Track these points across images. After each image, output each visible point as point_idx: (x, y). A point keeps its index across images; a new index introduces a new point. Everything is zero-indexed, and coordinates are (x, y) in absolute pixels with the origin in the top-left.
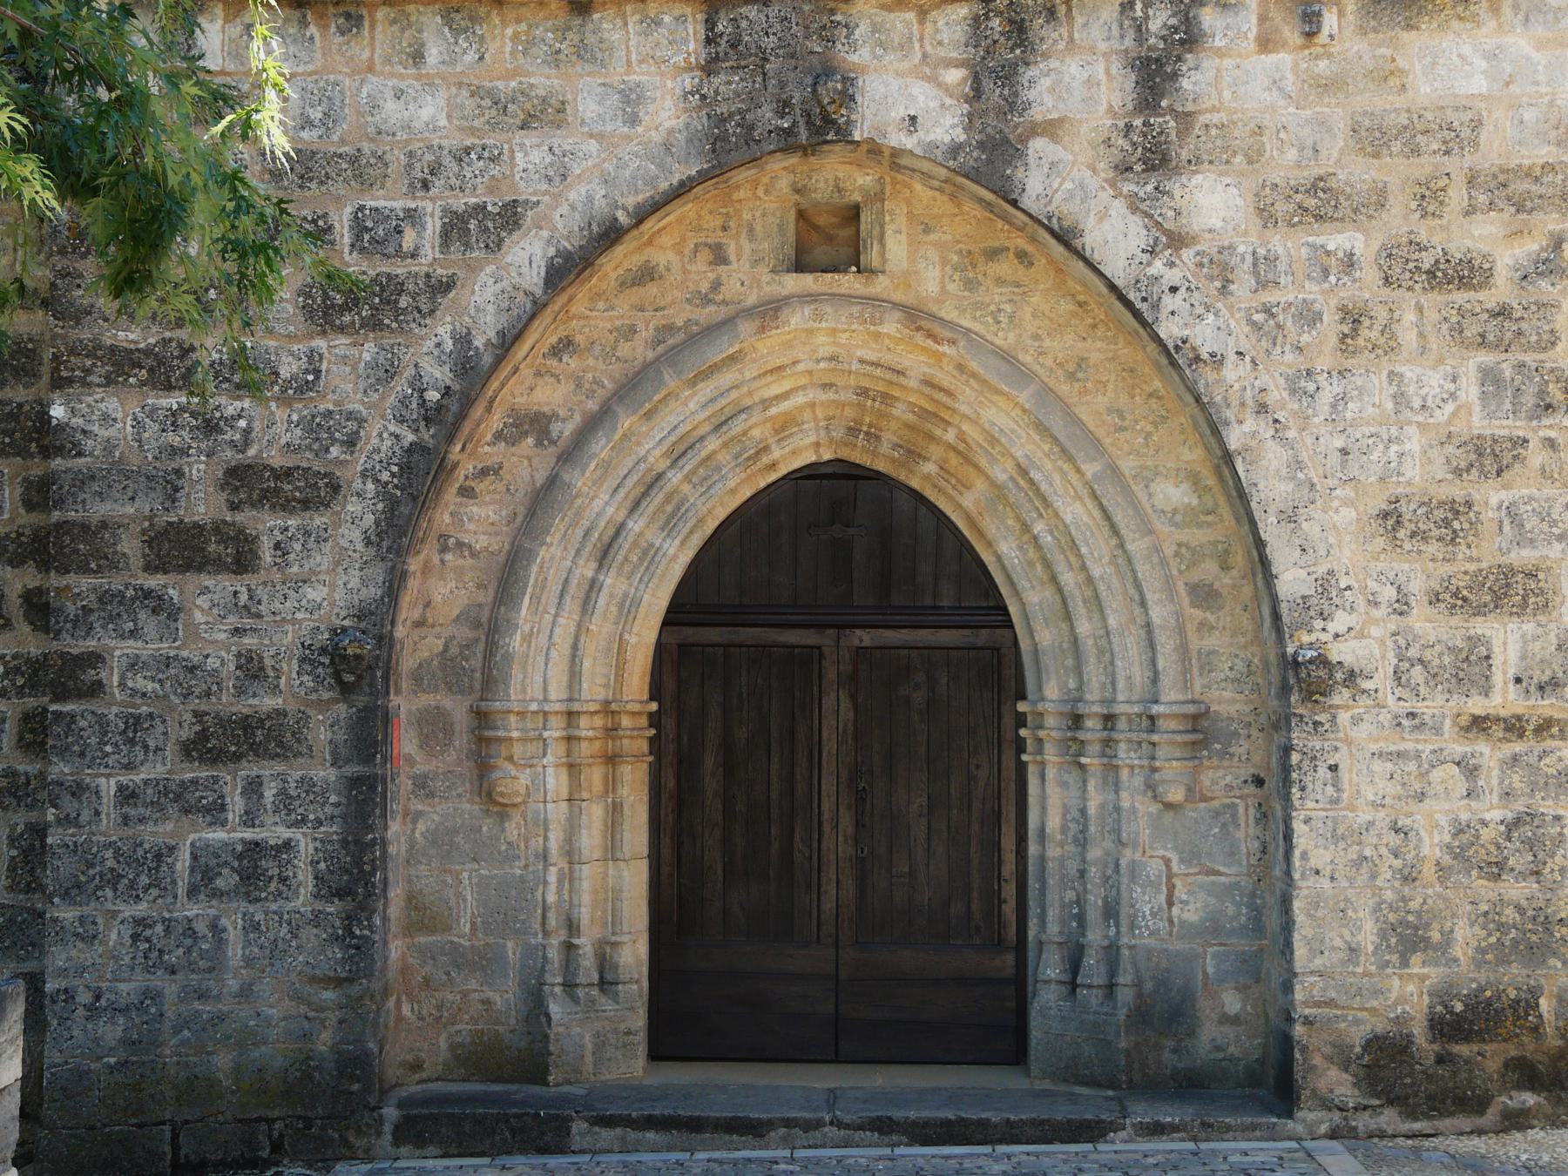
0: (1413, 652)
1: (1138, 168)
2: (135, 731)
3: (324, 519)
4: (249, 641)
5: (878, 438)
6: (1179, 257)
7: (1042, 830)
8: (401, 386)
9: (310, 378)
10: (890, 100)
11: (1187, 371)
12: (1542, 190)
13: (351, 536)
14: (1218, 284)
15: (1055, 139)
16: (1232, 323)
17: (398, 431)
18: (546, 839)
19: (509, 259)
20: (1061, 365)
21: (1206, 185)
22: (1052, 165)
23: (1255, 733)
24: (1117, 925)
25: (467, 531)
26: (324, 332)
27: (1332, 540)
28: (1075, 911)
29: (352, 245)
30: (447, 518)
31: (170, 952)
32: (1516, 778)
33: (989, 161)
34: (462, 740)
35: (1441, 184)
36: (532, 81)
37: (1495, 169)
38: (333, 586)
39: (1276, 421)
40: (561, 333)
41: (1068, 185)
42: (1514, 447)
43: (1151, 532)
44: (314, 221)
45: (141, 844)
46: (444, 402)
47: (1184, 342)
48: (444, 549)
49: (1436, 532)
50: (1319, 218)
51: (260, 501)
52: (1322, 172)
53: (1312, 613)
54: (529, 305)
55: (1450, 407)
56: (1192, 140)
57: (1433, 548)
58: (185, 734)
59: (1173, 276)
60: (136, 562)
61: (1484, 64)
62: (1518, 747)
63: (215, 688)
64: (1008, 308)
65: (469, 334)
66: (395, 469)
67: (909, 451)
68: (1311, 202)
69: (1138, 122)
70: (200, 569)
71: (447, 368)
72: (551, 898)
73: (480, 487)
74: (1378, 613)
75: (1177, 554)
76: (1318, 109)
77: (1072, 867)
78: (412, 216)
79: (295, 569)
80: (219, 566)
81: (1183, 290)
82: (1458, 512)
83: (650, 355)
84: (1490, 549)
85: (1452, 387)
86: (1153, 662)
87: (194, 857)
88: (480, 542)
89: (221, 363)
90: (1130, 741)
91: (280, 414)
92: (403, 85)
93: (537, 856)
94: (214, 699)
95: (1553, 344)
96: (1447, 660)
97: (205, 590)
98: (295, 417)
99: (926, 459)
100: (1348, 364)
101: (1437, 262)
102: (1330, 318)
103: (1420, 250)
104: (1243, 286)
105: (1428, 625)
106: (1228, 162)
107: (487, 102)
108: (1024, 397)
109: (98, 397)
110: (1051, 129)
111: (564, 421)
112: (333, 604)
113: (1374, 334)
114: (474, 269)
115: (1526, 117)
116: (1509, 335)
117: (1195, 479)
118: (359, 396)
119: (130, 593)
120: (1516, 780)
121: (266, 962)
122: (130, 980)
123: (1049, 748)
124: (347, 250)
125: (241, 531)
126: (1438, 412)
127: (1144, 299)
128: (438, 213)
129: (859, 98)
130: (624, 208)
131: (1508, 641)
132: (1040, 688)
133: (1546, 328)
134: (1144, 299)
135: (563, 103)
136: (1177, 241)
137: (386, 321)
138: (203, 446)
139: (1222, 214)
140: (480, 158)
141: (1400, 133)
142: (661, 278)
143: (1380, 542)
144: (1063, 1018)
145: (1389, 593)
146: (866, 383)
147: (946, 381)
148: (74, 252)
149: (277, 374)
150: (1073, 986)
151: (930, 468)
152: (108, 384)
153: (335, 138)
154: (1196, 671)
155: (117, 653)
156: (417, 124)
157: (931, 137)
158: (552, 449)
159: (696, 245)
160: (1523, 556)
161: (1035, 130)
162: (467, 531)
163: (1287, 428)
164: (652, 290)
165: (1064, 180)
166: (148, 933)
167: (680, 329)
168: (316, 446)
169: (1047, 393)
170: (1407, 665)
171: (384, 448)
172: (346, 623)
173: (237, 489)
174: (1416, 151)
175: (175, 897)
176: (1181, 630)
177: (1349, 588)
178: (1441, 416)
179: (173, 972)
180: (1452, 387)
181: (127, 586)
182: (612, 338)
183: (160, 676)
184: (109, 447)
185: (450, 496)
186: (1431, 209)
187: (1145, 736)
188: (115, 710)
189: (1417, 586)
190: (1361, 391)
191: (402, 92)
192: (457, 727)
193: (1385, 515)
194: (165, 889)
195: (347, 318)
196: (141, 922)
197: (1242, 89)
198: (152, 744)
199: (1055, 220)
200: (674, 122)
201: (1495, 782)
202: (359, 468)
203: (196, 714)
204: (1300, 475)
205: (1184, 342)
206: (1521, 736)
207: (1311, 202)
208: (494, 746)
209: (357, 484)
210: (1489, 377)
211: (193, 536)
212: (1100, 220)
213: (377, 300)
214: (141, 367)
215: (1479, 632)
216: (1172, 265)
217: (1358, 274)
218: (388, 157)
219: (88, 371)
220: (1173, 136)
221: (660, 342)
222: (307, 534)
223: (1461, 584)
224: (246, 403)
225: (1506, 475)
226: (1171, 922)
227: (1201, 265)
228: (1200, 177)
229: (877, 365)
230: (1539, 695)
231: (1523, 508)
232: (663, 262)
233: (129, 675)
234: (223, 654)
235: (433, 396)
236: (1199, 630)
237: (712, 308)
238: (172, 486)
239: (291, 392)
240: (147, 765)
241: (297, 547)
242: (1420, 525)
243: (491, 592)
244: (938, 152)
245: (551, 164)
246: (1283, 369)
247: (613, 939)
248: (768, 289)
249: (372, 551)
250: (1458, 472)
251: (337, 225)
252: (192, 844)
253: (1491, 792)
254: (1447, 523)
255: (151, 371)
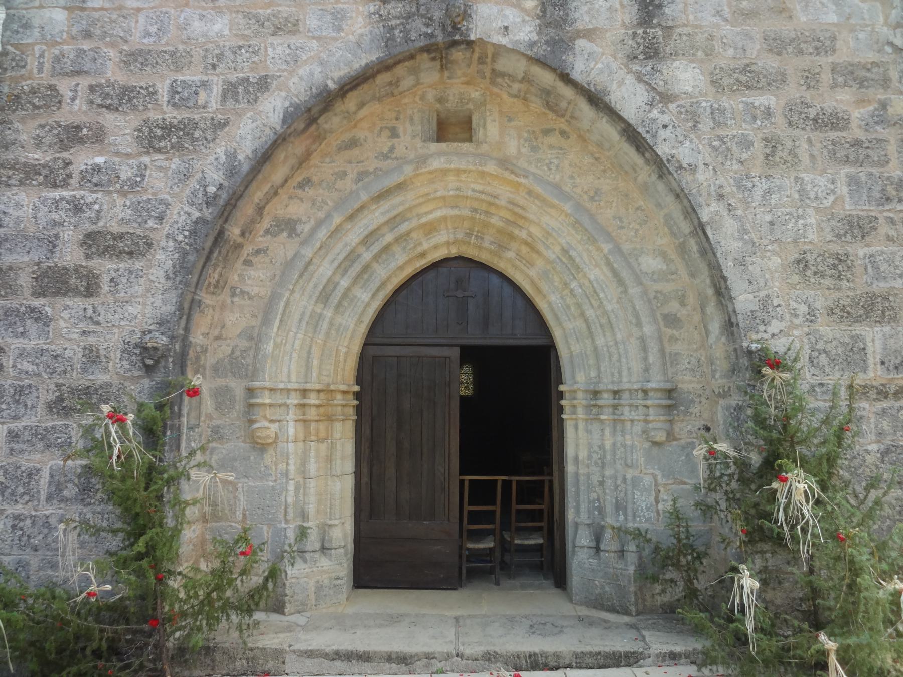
0: (820, 346)
1: (641, 57)
2: (20, 395)
3: (142, 264)
4: (91, 339)
5: (482, 238)
6: (667, 108)
7: (576, 459)
8: (193, 183)
9: (139, 179)
10: (492, 17)
11: (675, 175)
12: (873, 76)
13: (157, 274)
14: (691, 124)
15: (591, 40)
16: (701, 147)
17: (190, 210)
18: (288, 464)
19: (261, 109)
20: (586, 192)
21: (681, 66)
22: (590, 54)
23: (704, 400)
24: (625, 515)
25: (247, 285)
26: (148, 153)
27: (767, 276)
28: (597, 505)
29: (169, 102)
30: (236, 278)
31: (35, 537)
32: (885, 423)
33: (553, 52)
34: (239, 406)
35: (817, 71)
36: (280, 8)
37: (846, 63)
38: (144, 305)
39: (730, 204)
40: (304, 175)
41: (600, 66)
42: (870, 222)
43: (641, 284)
44: (147, 88)
45: (19, 467)
46: (219, 193)
47: (673, 157)
48: (233, 295)
49: (829, 272)
50: (748, 87)
51: (103, 253)
52: (748, 61)
53: (758, 322)
54: (272, 135)
55: (831, 198)
56: (672, 42)
57: (828, 282)
58: (51, 397)
59: (665, 119)
60: (27, 292)
61: (834, 7)
62: (885, 404)
63: (69, 368)
64: (556, 161)
65: (235, 152)
66: (187, 233)
67: (499, 245)
68: (744, 78)
69: (640, 31)
70: (65, 295)
71: (221, 173)
72: (290, 500)
73: (255, 260)
74: (797, 322)
75: (655, 298)
76: (744, 27)
77: (596, 479)
78: (204, 84)
79: (122, 294)
80: (77, 293)
81: (670, 127)
82: (840, 260)
83: (354, 187)
84: (861, 283)
85: (832, 187)
86: (645, 359)
87: (52, 476)
88: (254, 291)
89: (87, 171)
90: (631, 405)
91: (120, 201)
92: (204, 13)
93: (282, 474)
94: (68, 376)
95: (887, 163)
96: (840, 350)
97: (67, 308)
98: (128, 203)
99: (509, 250)
100: (770, 172)
101: (818, 114)
102: (758, 146)
103: (808, 108)
104: (706, 125)
105: (828, 330)
106: (693, 55)
107: (253, 21)
108: (568, 207)
109: (14, 192)
110: (588, 34)
111: (304, 223)
112: (144, 316)
113: (784, 154)
114: (239, 115)
115: (860, 36)
116: (861, 157)
117: (664, 255)
118: (168, 190)
119: (23, 309)
120: (886, 425)
121: (93, 544)
122: (10, 555)
123: (580, 410)
124: (165, 104)
125: (91, 272)
126: (825, 201)
127: (648, 132)
128: (220, 83)
129: (474, 16)
130: (332, 79)
131: (875, 338)
132: (574, 377)
133: (883, 153)
134: (648, 132)
135: (297, 20)
136: (666, 98)
137: (186, 146)
138: (72, 220)
139: (692, 84)
140: (247, 52)
141: (791, 41)
142: (361, 145)
143: (796, 279)
144: (593, 570)
145: (803, 309)
146: (476, 205)
147: (521, 202)
148: (9, 109)
149: (119, 177)
150: (598, 549)
151: (511, 254)
152: (20, 185)
153: (163, 42)
154: (668, 364)
155: (12, 347)
156: (211, 33)
157: (517, 38)
158: (297, 239)
159: (381, 128)
160: (880, 287)
161: (580, 34)
162: (247, 285)
163: (736, 208)
164: (356, 152)
165: (597, 63)
166: (21, 524)
167: (371, 173)
168: (139, 220)
169: (579, 206)
170: (817, 353)
171: (180, 221)
172: (152, 328)
173: (90, 246)
174: (801, 52)
175: (39, 502)
176: (660, 339)
177: (779, 306)
178: (827, 203)
179: (36, 550)
180: (832, 187)
181: (21, 305)
182: (333, 178)
183: (37, 361)
184: (18, 221)
185: (239, 264)
186: (812, 84)
187: (641, 402)
188: (9, 382)
189: (819, 305)
190: (780, 188)
191: (204, 16)
192: (238, 398)
193: (799, 262)
194: (33, 496)
195: (162, 144)
196: (17, 517)
197: (700, 14)
198: (29, 404)
199: (592, 86)
200: (363, 30)
201: (873, 426)
202: (165, 233)
203: (57, 385)
204: (746, 237)
205: (673, 157)
206: (886, 397)
207: (744, 78)
208: (256, 409)
209: (163, 243)
210: (853, 181)
211: (62, 275)
212: (619, 86)
213: (181, 133)
214: (40, 174)
215: (858, 333)
216: (663, 112)
217: (773, 120)
218: (193, 52)
219: (9, 177)
220: (661, 40)
221: (359, 180)
222: (131, 273)
223: (846, 304)
224: (99, 195)
225: (867, 238)
226: (658, 512)
227: (681, 113)
228: (678, 62)
229: (482, 192)
230: (895, 371)
231: (878, 258)
232: (363, 137)
233: (19, 360)
234: (75, 347)
235: (212, 189)
236: (669, 341)
237: (390, 161)
238: (52, 243)
239: (126, 187)
240: (26, 417)
241: (124, 281)
242: (819, 267)
243: (260, 319)
244: (522, 46)
245: (289, 54)
246: (732, 174)
247: (330, 522)
248: (420, 151)
249: (170, 283)
250: (838, 236)
251: (160, 90)
252: (51, 468)
253: (871, 433)
254: (835, 266)
255: (46, 176)
